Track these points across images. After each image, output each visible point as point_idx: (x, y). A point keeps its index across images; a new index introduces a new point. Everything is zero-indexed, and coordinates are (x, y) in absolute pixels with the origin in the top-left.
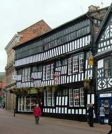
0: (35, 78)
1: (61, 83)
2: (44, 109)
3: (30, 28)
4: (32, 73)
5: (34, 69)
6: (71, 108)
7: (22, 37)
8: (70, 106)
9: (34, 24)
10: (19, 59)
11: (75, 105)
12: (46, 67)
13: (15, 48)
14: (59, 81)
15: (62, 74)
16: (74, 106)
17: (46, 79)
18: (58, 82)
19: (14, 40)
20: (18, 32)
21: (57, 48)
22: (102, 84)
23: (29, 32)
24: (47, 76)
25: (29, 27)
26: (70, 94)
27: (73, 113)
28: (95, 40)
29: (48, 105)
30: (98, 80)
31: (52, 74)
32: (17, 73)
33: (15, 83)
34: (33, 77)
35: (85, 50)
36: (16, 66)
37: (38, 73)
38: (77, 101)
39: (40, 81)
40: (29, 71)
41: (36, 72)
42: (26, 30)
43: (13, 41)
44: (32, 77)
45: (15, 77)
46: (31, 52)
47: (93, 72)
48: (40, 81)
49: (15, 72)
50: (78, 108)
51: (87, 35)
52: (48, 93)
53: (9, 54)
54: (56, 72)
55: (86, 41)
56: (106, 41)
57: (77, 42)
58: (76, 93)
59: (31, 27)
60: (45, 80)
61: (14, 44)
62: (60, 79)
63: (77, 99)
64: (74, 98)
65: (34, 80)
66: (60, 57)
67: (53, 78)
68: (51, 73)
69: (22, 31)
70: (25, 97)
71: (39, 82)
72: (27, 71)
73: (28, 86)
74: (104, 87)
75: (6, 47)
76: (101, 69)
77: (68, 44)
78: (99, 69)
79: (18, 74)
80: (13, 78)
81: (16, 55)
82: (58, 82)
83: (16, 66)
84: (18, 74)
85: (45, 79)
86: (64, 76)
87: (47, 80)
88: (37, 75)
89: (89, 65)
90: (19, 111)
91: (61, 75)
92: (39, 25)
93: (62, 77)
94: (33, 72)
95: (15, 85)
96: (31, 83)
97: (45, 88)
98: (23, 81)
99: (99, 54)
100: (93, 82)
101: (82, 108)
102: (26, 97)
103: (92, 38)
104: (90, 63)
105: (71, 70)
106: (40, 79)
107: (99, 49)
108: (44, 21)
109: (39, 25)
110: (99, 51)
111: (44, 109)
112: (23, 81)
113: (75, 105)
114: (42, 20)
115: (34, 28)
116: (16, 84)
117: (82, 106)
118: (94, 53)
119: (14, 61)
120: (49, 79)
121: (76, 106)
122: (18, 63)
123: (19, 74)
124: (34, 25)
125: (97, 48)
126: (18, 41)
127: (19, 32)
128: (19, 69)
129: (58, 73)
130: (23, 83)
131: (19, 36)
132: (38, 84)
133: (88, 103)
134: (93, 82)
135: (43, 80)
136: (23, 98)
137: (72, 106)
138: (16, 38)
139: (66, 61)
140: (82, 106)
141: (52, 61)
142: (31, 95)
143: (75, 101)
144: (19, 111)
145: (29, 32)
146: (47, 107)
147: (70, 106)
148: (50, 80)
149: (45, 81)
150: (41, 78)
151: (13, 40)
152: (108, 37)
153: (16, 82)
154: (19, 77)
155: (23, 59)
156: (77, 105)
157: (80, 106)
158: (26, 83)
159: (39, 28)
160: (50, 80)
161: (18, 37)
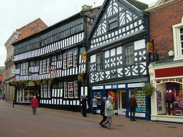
0: (32, 72)
1: (57, 77)
2: (41, 100)
3: (27, 26)
4: (30, 67)
5: (32, 63)
6: (66, 100)
7: (20, 34)
8: (65, 97)
9: (32, 22)
10: (17, 55)
11: (70, 97)
12: (42, 62)
13: (14, 44)
14: (55, 75)
15: (57, 68)
16: (69, 97)
17: (43, 73)
18: (54, 75)
19: (13, 36)
20: (17, 30)
21: (53, 44)
22: (95, 77)
23: (27, 30)
24: (43, 70)
25: (27, 25)
26: (65, 87)
27: (68, 104)
28: (88, 37)
29: (44, 97)
30: (91, 74)
31: (48, 68)
32: (16, 67)
33: (14, 76)
34: (31, 71)
35: (79, 46)
36: (14, 61)
37: (36, 67)
38: (71, 93)
39: (37, 74)
40: (27, 66)
41: (34, 66)
42: (24, 27)
43: (12, 38)
44: (30, 71)
45: (14, 71)
46: (29, 48)
47: (86, 66)
48: (37, 74)
49: (14, 66)
50: (72, 100)
51: (81, 32)
52: (45, 86)
53: (9, 50)
54: (52, 67)
55: (80, 38)
56: (98, 37)
57: (71, 38)
58: (71, 86)
59: (29, 25)
60: (41, 73)
61: (13, 41)
62: (55, 72)
63: (71, 91)
64: (69, 90)
65: (31, 74)
66: (56, 53)
67: (49, 72)
68: (48, 67)
69: (20, 29)
70: (23, 89)
71: (36, 75)
72: (25, 66)
73: (26, 79)
74: (96, 80)
75: (6, 43)
76: (94, 63)
77: (63, 41)
78: (92, 64)
79: (16, 68)
80: (13, 72)
81: (15, 50)
82: (54, 75)
83: (14, 61)
84: (16, 68)
85: (42, 73)
86: (59, 70)
87: (44, 74)
88: (34, 69)
89: (82, 60)
90: (17, 102)
91: (57, 69)
92: (36, 23)
93: (57, 71)
94: (31, 67)
95: (14, 78)
96: (29, 76)
97: (42, 81)
98: (21, 75)
99: (92, 50)
100: (86, 76)
101: (76, 100)
102: (24, 90)
103: (86, 35)
104: (83, 58)
105: (65, 64)
106: (37, 73)
107: (92, 45)
108: (40, 19)
109: (36, 23)
110: (92, 47)
111: (41, 100)
112: (21, 75)
113: (70, 97)
114: (39, 18)
115: (32, 26)
116: (15, 77)
117: (76, 97)
118: (88, 49)
119: (13, 56)
120: (46, 73)
121: (71, 97)
122: (17, 58)
123: (18, 69)
124: (32, 23)
125: (90, 44)
126: (17, 38)
127: (18, 29)
128: (18, 64)
129: (54, 67)
130: (22, 76)
131: (17, 34)
132: (35, 77)
133: (81, 95)
134: (86, 76)
135: (40, 74)
136: (21, 90)
137: (67, 98)
138: (15, 35)
139: (61, 56)
140: (76, 97)
141: (48, 56)
142: (29, 87)
143: (70, 93)
144: (17, 102)
145: (27, 30)
146: (44, 99)
147: (65, 97)
148: (46, 74)
149: (42, 74)
150: (38, 72)
151: (12, 36)
152: (100, 34)
153: (14, 75)
154: (18, 71)
155: (22, 54)
156: (72, 97)
157: (74, 97)
158: (24, 76)
159: (36, 26)
160: (46, 74)
161: (16, 34)
